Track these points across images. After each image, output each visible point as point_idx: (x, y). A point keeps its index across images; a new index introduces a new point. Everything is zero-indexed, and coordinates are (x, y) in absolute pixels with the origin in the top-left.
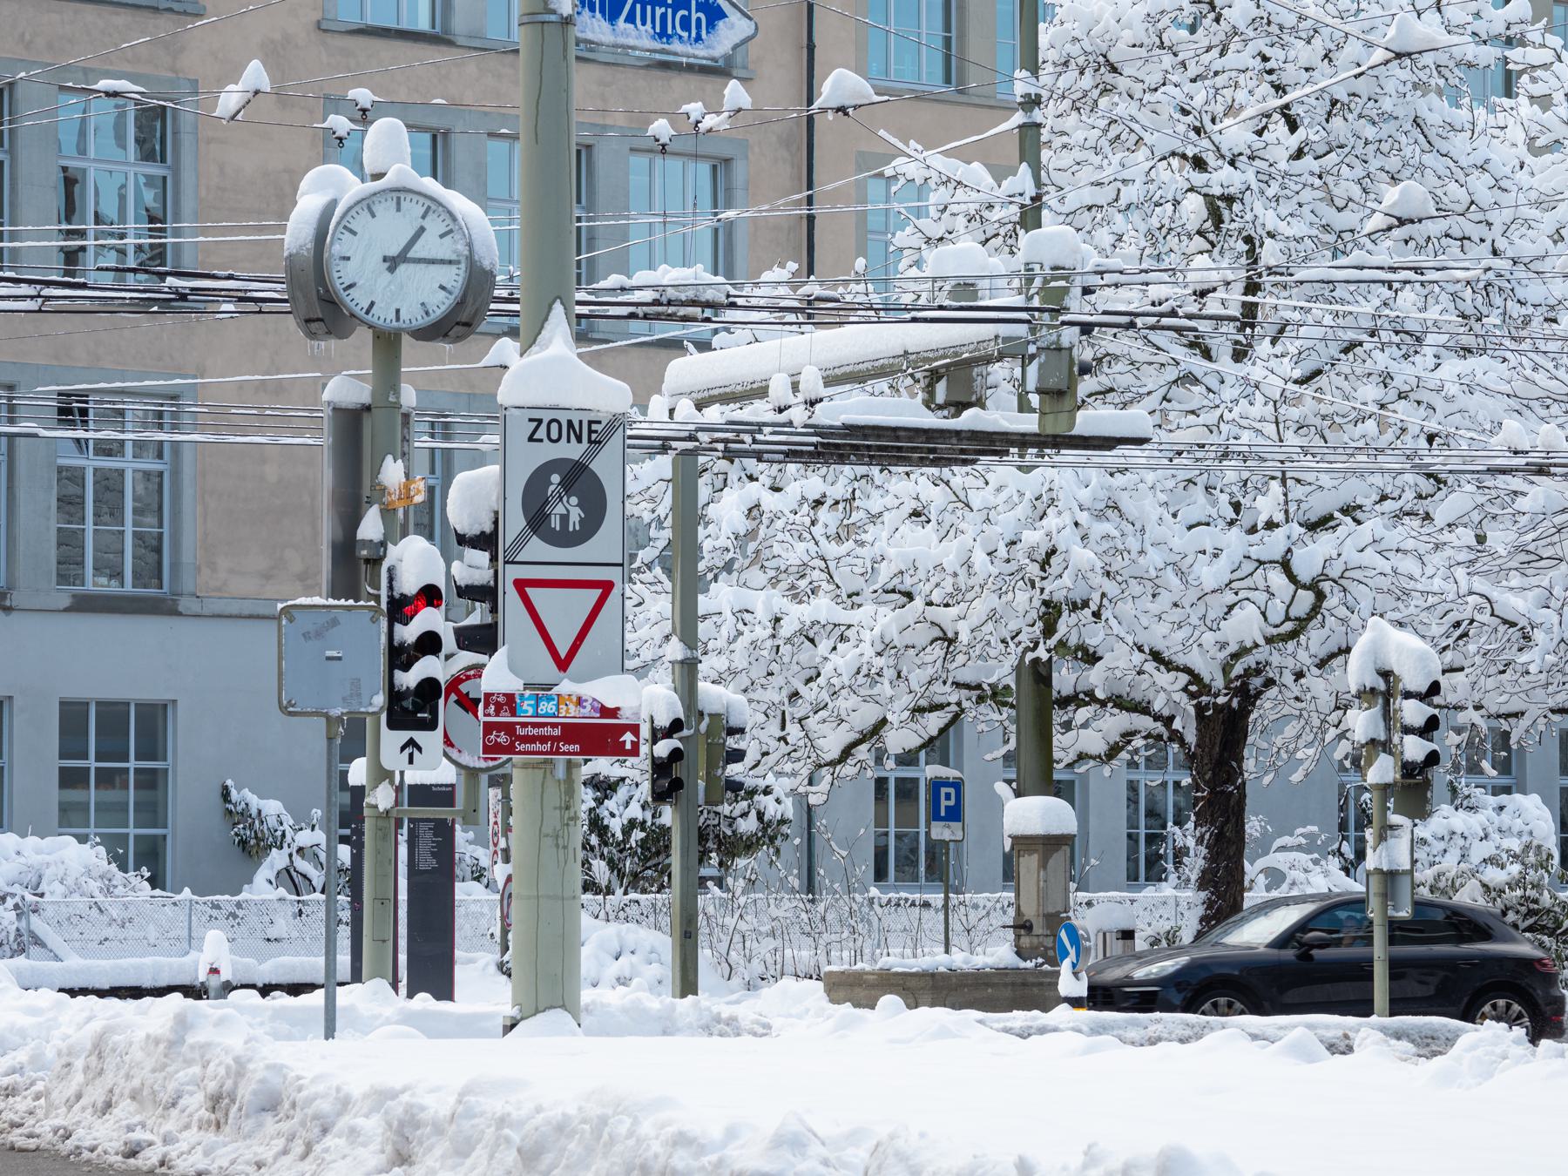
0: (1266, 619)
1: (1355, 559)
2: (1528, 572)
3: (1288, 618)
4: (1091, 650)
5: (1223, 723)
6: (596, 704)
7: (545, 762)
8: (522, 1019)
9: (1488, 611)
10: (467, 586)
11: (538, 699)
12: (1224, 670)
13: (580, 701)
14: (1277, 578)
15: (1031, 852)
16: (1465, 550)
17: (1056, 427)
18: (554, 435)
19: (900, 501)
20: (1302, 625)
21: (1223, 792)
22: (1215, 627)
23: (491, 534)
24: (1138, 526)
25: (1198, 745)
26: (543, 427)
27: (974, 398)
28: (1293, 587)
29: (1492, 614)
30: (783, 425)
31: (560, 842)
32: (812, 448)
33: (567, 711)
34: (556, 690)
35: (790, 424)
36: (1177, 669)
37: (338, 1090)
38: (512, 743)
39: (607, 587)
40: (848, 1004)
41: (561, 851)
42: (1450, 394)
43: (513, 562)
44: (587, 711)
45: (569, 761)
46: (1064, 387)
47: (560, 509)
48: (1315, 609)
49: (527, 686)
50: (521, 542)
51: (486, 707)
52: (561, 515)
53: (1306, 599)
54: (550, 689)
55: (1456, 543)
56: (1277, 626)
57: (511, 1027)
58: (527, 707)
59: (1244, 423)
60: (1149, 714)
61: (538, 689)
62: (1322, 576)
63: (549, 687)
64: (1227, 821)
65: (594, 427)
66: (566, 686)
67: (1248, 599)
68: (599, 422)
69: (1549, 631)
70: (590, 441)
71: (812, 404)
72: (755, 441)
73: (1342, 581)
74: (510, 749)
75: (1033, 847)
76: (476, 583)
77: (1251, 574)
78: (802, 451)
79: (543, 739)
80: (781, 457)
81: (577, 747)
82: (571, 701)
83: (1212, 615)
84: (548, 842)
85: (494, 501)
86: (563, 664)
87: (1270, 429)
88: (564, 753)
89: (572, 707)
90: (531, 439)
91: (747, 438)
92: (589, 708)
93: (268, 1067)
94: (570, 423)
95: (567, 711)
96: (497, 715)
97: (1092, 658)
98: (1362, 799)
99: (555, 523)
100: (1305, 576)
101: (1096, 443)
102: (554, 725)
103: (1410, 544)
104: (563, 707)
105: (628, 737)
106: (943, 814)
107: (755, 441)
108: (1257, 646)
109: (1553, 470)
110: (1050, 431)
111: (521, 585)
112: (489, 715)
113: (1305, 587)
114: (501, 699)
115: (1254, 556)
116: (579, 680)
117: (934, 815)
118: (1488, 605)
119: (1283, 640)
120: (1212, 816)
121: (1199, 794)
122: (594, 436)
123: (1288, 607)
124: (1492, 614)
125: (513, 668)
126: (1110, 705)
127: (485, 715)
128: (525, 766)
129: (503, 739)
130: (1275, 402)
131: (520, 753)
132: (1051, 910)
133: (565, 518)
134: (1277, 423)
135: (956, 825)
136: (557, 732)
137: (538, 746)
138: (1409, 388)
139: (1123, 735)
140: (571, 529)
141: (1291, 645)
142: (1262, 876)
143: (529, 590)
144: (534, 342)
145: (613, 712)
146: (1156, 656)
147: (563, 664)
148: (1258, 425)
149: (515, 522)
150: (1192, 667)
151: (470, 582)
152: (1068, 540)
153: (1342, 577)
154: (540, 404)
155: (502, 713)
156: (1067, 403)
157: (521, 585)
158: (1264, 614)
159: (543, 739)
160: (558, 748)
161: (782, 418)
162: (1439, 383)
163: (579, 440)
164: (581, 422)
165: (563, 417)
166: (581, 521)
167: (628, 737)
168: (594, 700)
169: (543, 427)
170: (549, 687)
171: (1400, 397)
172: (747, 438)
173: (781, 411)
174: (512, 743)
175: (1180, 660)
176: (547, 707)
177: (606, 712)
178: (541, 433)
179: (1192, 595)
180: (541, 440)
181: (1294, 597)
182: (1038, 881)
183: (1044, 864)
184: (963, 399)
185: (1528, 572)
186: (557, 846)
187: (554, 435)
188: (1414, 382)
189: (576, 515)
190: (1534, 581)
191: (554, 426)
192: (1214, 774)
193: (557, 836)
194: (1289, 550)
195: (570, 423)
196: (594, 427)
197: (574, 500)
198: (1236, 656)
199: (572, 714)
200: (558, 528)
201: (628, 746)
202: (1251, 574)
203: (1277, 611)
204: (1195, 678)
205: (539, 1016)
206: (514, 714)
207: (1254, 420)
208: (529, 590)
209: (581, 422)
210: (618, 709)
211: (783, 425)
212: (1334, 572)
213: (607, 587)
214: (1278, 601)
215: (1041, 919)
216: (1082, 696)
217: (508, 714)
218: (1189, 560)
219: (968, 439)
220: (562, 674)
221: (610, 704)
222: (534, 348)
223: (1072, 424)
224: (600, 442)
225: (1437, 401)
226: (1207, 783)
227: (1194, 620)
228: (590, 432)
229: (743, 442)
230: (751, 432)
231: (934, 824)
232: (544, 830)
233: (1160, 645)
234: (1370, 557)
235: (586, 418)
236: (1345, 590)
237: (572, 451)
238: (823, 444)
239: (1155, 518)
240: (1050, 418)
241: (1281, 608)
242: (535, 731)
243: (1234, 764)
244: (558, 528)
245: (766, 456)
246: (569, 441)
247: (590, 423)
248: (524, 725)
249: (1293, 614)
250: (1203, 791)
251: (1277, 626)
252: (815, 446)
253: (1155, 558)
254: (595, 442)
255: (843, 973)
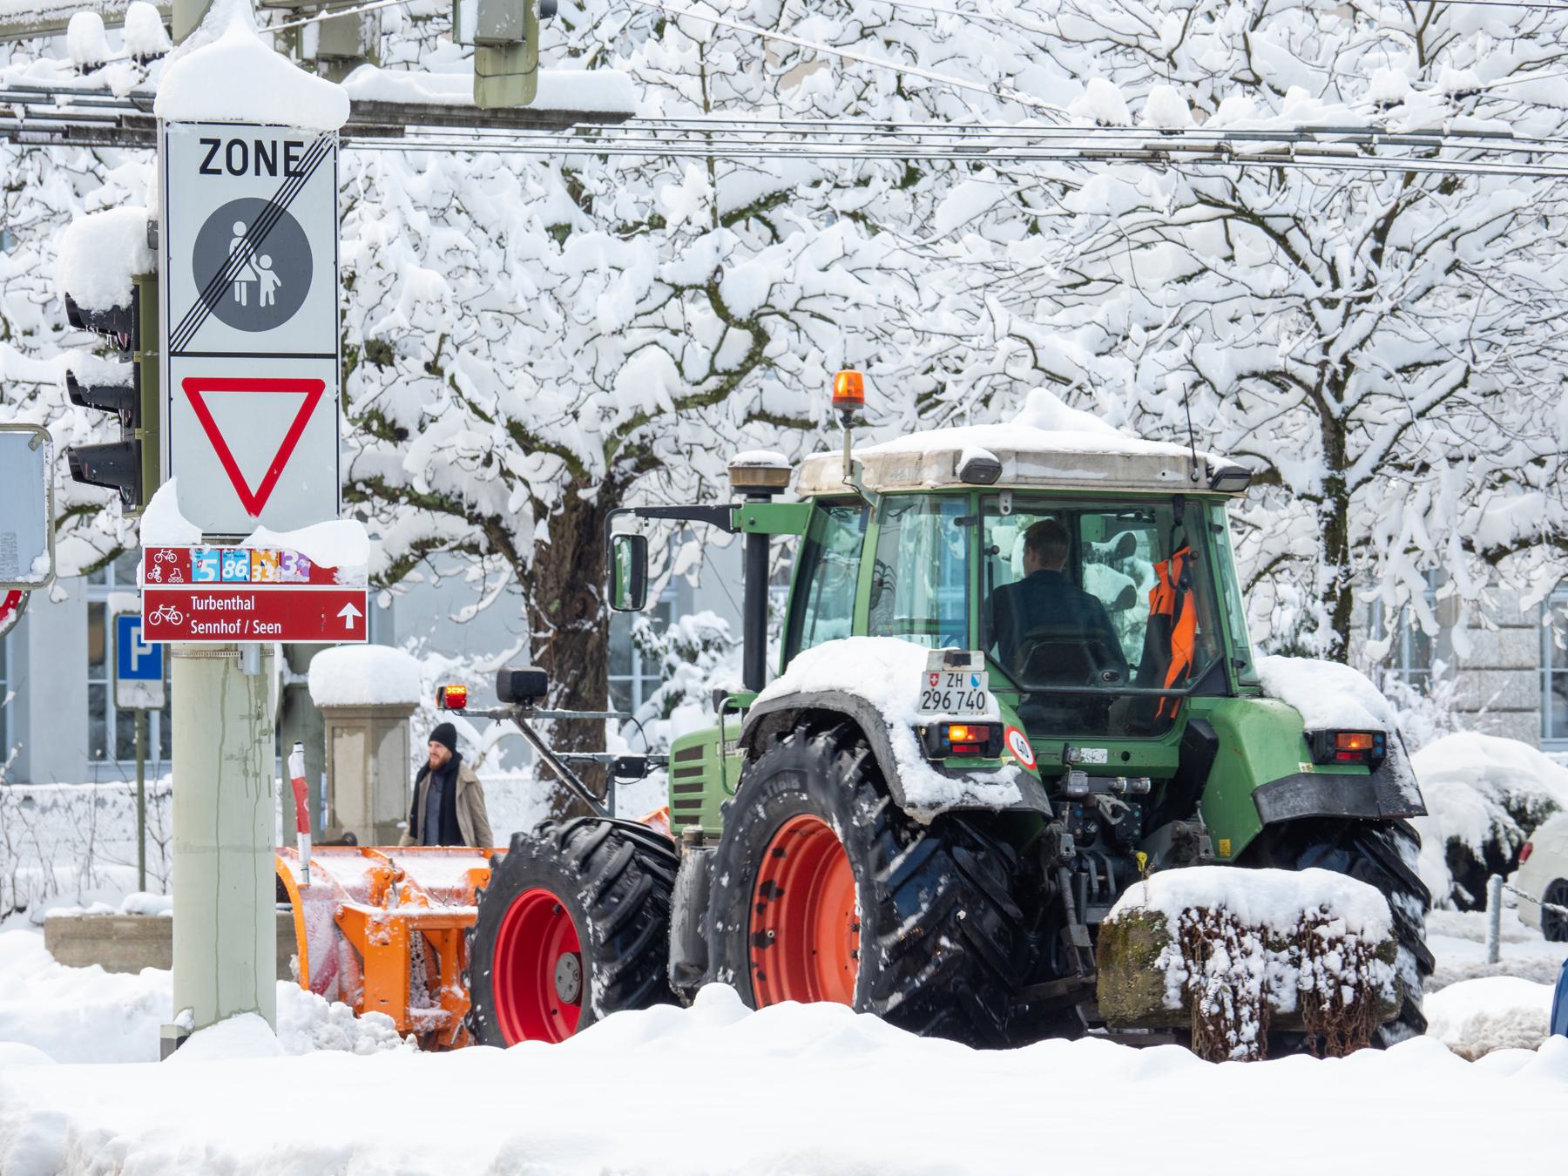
0: (682, 373)
1: (817, 282)
2: (1066, 300)
3: (713, 372)
4: (389, 420)
5: (577, 526)
6: (304, 564)
7: (227, 649)
8: (195, 1029)
9: (1029, 361)
10: (93, 388)
11: (222, 556)
12: (605, 448)
13: (281, 559)
14: (700, 312)
15: (353, 729)
16: (980, 268)
17: (507, 96)
18: (237, 165)
19: (126, 193)
20: (733, 378)
21: (576, 631)
22: (608, 387)
23: (128, 309)
24: (494, 234)
25: (538, 560)
26: (222, 151)
27: (361, 51)
28: (721, 324)
29: (1035, 367)
30: (96, 92)
31: (250, 766)
32: (113, 125)
33: (263, 574)
34: (247, 543)
35: (106, 90)
36: (547, 448)
37: (209, 1152)
38: (187, 622)
39: (314, 388)
40: (97, 967)
41: (251, 780)
42: (947, 31)
43: (182, 354)
44: (291, 573)
45: (262, 647)
46: (516, 36)
47: (246, 274)
48: (755, 357)
49: (208, 537)
50: (192, 323)
51: (149, 568)
52: (248, 283)
53: (741, 340)
54: (239, 542)
55: (967, 258)
56: (697, 383)
57: (174, 1043)
58: (206, 569)
59: (652, 75)
60: (461, 513)
61: (223, 542)
62: (769, 308)
63: (236, 539)
64: (582, 676)
65: (293, 151)
66: (262, 537)
67: (655, 343)
68: (300, 144)
69: (1120, 391)
70: (288, 173)
71: (145, 61)
72: (28, 115)
73: (794, 316)
74: (183, 632)
75: (358, 722)
76: (107, 383)
77: (663, 305)
78: (88, 129)
79: (230, 616)
80: (46, 136)
81: (277, 627)
82: (269, 559)
83: (604, 368)
84: (234, 767)
85: (134, 261)
86: (254, 504)
87: (692, 86)
88: (260, 636)
89: (270, 567)
90: (204, 169)
91: (18, 109)
92: (294, 568)
93: (38, 1118)
94: (259, 146)
95: (263, 574)
96: (165, 581)
97: (398, 434)
98: (636, 627)
99: (240, 295)
100: (740, 310)
101: (555, 119)
102: (245, 595)
103: (897, 260)
104: (256, 567)
105: (349, 612)
106: (135, 667)
107: (28, 115)
108: (660, 411)
109: (1173, 155)
110: (493, 102)
111: (193, 387)
112: (153, 581)
113: (740, 324)
114: (170, 557)
115: (668, 279)
116: (279, 527)
117: (124, 672)
118: (1029, 353)
119: (701, 404)
120: (560, 666)
121: (541, 635)
122: (293, 165)
123: (714, 354)
124: (1035, 367)
125: (185, 512)
126: (403, 499)
127: (148, 581)
128: (195, 655)
129: (173, 616)
130: (702, 45)
131: (198, 636)
132: (385, 817)
133: (254, 288)
134: (703, 76)
135: (155, 685)
136: (249, 605)
137: (221, 627)
138: (878, 22)
139: (415, 546)
140: (263, 304)
141: (713, 412)
142: (495, 749)
143: (204, 394)
144: (200, 23)
145: (324, 575)
146: (516, 430)
147: (254, 504)
148: (672, 79)
149: (181, 293)
150: (569, 446)
151: (97, 382)
152: (399, 255)
153: (795, 309)
154: (218, 118)
155: (172, 578)
156: (521, 62)
157: (193, 387)
158: (679, 365)
159: (230, 616)
160: (251, 628)
161: (93, 80)
162: (929, 15)
163: (273, 171)
164: (274, 144)
165: (250, 139)
166: (277, 291)
167: (349, 612)
168: (302, 556)
169: (222, 151)
170: (236, 539)
171: (863, 36)
172: (18, 109)
173: (87, 70)
174: (187, 622)
175: (551, 435)
176: (236, 569)
177: (321, 575)
178: (219, 162)
179: (577, 337)
180: (218, 172)
181: (722, 339)
182: (365, 773)
183: (373, 749)
184: (347, 52)
185: (1066, 300)
186: (246, 773)
187: (237, 165)
188: (886, 11)
189: (269, 283)
190: (1079, 314)
191: (237, 151)
192: (563, 604)
193: (245, 760)
194: (719, 269)
195: (259, 146)
196: (293, 151)
197: (266, 261)
198: (625, 428)
199: (271, 578)
200: (244, 303)
201: (350, 625)
202: (663, 305)
203: (697, 365)
204: (572, 462)
205: (223, 1024)
206: (188, 580)
207: (669, 71)
208: (204, 394)
209: (274, 144)
210: (335, 569)
211: (96, 92)
212: (783, 302)
213: (314, 388)
214: (698, 345)
215: (370, 831)
216: (360, 487)
217: (179, 579)
218: (571, 285)
219: (369, 113)
220: (253, 519)
221: (324, 563)
222: (200, 34)
223: (531, 90)
224: (301, 174)
225: (920, 41)
226: (552, 617)
227: (581, 375)
228: (288, 158)
229: (12, 115)
230: (24, 102)
231: (121, 682)
232: (227, 750)
233: (522, 415)
234: (839, 279)
235: (281, 137)
236: (798, 329)
237: (264, 187)
238: (130, 119)
239: (520, 221)
240: (492, 83)
241: (705, 357)
242: (219, 605)
243: (593, 588)
244: (244, 303)
245: (23, 135)
246: (258, 173)
247: (288, 145)
248: (203, 595)
249: (719, 366)
250: (547, 629)
251: (697, 383)
252: (119, 122)
253: (524, 281)
254: (295, 174)
255: (79, 919)
